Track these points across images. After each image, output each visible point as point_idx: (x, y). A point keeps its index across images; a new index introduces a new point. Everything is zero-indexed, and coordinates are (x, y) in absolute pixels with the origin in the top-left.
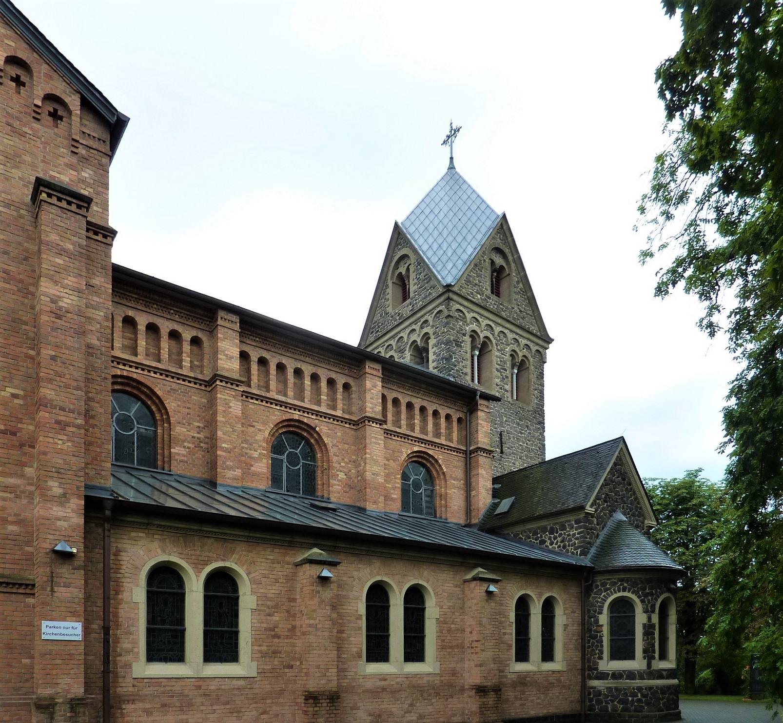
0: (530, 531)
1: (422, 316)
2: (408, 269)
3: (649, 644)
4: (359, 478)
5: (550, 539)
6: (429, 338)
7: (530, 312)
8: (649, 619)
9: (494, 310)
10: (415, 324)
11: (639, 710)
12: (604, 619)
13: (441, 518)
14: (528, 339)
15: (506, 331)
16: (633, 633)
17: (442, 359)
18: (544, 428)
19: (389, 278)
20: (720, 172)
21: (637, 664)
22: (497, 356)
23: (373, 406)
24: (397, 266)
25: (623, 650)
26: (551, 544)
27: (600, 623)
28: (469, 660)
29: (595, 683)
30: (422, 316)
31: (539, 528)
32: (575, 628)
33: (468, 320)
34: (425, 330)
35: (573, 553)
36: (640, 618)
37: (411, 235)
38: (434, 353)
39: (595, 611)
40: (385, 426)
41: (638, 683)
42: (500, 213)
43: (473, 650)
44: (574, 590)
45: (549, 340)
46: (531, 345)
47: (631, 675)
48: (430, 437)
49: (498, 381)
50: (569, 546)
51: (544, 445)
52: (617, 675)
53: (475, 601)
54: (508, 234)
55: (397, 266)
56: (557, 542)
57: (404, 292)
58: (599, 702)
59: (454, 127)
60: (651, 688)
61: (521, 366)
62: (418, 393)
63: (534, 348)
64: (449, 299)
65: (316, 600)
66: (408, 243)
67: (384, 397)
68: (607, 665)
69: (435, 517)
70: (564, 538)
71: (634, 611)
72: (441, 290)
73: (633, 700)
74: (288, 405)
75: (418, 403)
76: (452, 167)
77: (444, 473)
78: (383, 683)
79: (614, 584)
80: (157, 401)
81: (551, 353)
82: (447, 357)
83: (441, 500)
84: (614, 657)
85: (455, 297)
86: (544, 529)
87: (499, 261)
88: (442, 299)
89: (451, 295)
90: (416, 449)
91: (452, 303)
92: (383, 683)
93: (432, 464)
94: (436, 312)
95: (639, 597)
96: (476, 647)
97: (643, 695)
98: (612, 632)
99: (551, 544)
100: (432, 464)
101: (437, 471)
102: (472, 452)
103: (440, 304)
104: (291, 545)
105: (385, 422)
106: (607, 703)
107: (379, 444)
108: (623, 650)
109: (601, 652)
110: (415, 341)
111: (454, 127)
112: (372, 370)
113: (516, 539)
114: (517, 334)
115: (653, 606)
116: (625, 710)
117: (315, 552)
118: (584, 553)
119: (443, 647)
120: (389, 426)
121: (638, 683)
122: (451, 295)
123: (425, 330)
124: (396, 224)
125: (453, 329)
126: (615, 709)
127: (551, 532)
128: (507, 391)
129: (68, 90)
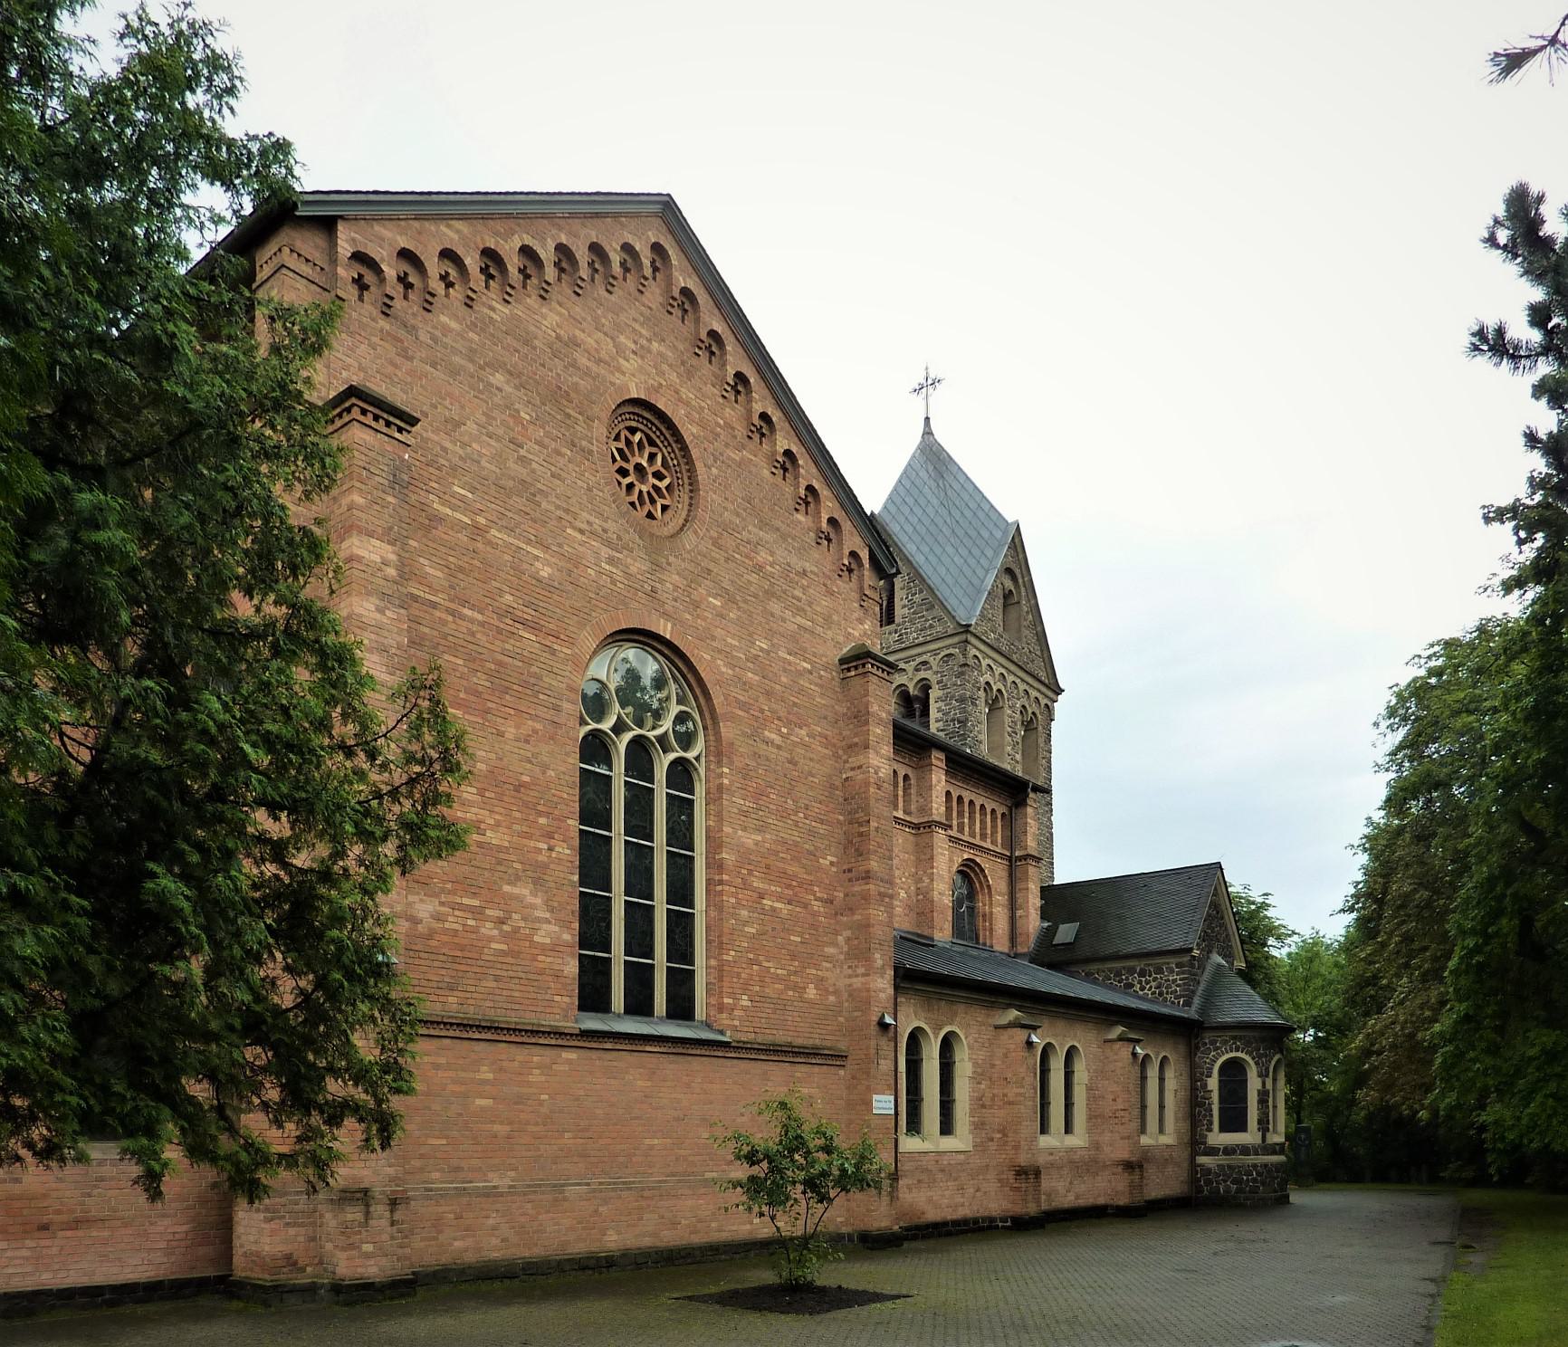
0: (1110, 970)
1: (919, 655)
3: (1264, 1113)
4: (921, 897)
5: (1140, 982)
7: (1039, 653)
8: (1264, 1084)
9: (1006, 653)
10: (906, 663)
11: (1254, 1191)
12: (1213, 1083)
13: (985, 944)
14: (1039, 691)
15: (1018, 681)
16: (1244, 1099)
17: (953, 720)
18: (1051, 810)
21: (1250, 1137)
22: (1010, 714)
23: (938, 809)
25: (1234, 1121)
26: (1142, 989)
27: (1209, 1088)
28: (1112, 1132)
29: (1202, 1160)
30: (919, 655)
31: (1124, 968)
32: (1183, 1094)
34: (922, 674)
35: (1173, 1003)
36: (1254, 1084)
38: (939, 710)
39: (1202, 1074)
40: (950, 832)
41: (1251, 1159)
43: (1117, 1120)
44: (1182, 1048)
45: (1059, 691)
46: (1040, 697)
47: (1245, 1150)
48: (977, 841)
49: (1009, 748)
50: (1167, 993)
51: (1052, 834)
52: (1229, 1151)
53: (1120, 1064)
54: (1019, 549)
56: (1151, 987)
58: (1209, 1182)
59: (932, 376)
60: (1266, 1166)
61: (1029, 726)
62: (968, 784)
63: (1044, 701)
64: (966, 641)
65: (1025, 1066)
67: (948, 793)
68: (1217, 1138)
69: (978, 943)
70: (1160, 983)
71: (1245, 1074)
72: (951, 628)
73: (1248, 1180)
75: (967, 796)
76: (928, 432)
77: (989, 886)
78: (1051, 1158)
79: (1225, 1042)
81: (1060, 707)
82: (961, 719)
83: (985, 921)
84: (1224, 1128)
85: (973, 640)
86: (1131, 971)
87: (1009, 584)
88: (956, 639)
90: (966, 856)
91: (969, 647)
92: (1051, 1158)
93: (976, 874)
94: (943, 654)
95: (1253, 1059)
96: (1122, 1117)
97: (1258, 1174)
98: (1222, 1099)
99: (1142, 989)
100: (976, 874)
101: (980, 883)
102: (1019, 858)
103: (953, 646)
104: (992, 1006)
105: (951, 827)
106: (1218, 1183)
107: (944, 855)
108: (1234, 1121)
109: (1211, 1123)
111: (932, 376)
112: (938, 758)
113: (1089, 977)
114: (1028, 684)
115: (1267, 1070)
116: (1239, 1191)
117: (1013, 1014)
118: (1188, 1004)
119: (1092, 1117)
120: (954, 833)
121: (1251, 1159)
125: (969, 682)
126: (1227, 1191)
127: (1142, 974)
128: (1017, 762)
129: (862, 544)
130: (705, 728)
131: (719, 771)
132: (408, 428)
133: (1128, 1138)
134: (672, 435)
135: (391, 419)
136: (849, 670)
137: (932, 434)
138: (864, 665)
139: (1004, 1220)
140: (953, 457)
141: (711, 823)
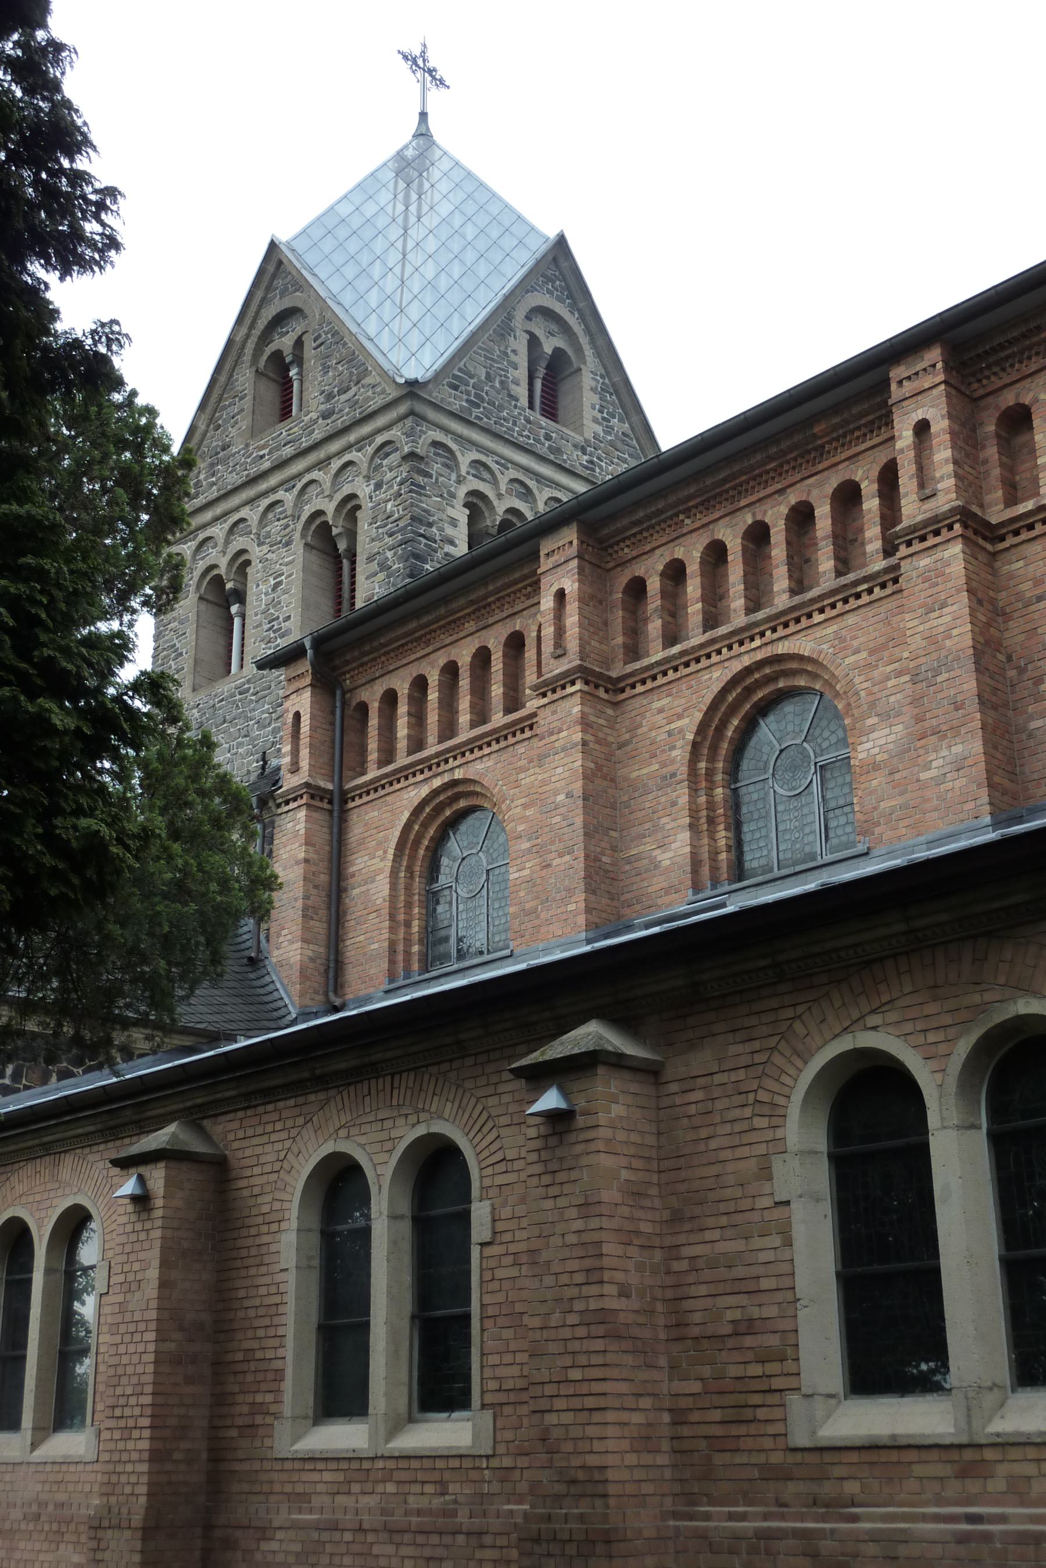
1: (237, 509)
2: (299, 343)
6: (358, 507)
19: (247, 357)
20: (167, 576)
24: (266, 336)
33: (464, 469)
34: (239, 542)
37: (311, 271)
42: (552, 234)
55: (266, 336)
57: (284, 402)
66: (300, 284)
72: (393, 394)
74: (859, 589)
76: (423, 133)
80: (767, 671)
85: (431, 414)
89: (420, 408)
110: (320, 513)
122: (420, 408)
123: (239, 542)
124: (273, 246)
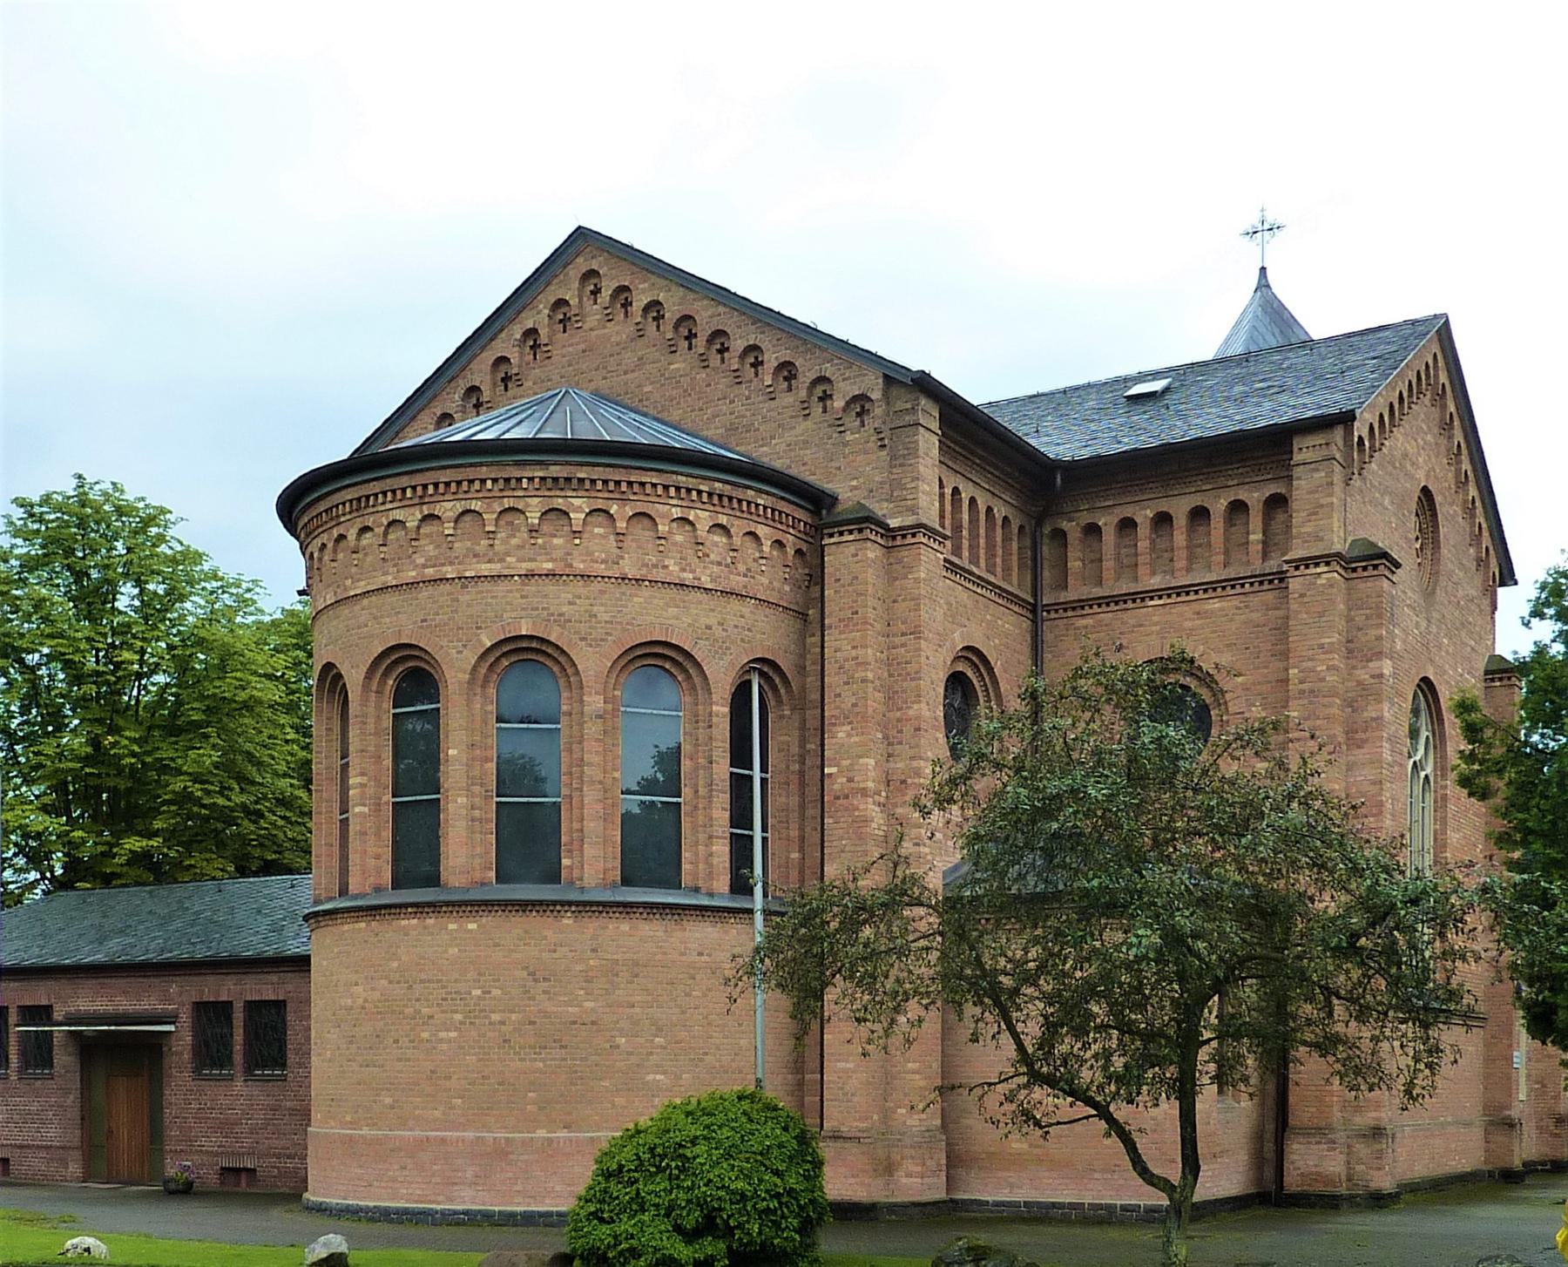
76: (1263, 284)
130: (1435, 747)
131: (1443, 783)
132: (1394, 569)
133: (930, 1078)
134: (1428, 505)
135: (1375, 562)
136: (1493, 680)
137: (1268, 286)
138: (1509, 678)
139: (1543, 1163)
140: (1297, 317)
141: (1438, 827)
